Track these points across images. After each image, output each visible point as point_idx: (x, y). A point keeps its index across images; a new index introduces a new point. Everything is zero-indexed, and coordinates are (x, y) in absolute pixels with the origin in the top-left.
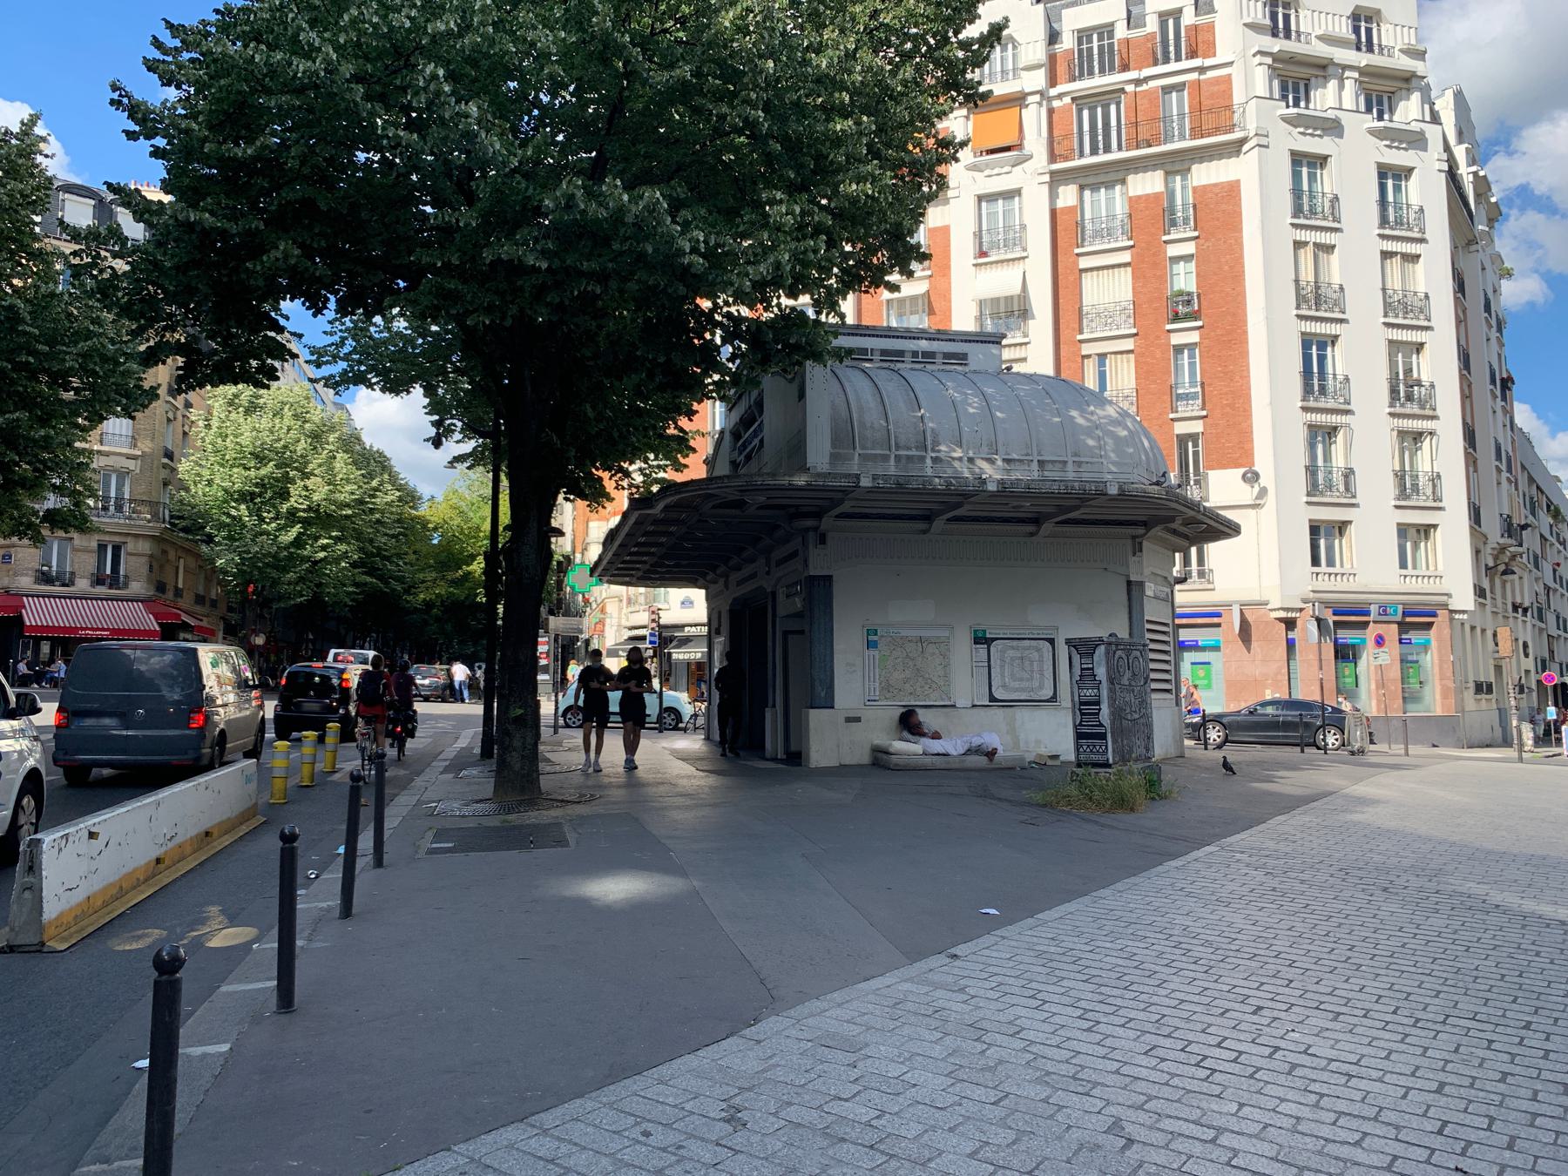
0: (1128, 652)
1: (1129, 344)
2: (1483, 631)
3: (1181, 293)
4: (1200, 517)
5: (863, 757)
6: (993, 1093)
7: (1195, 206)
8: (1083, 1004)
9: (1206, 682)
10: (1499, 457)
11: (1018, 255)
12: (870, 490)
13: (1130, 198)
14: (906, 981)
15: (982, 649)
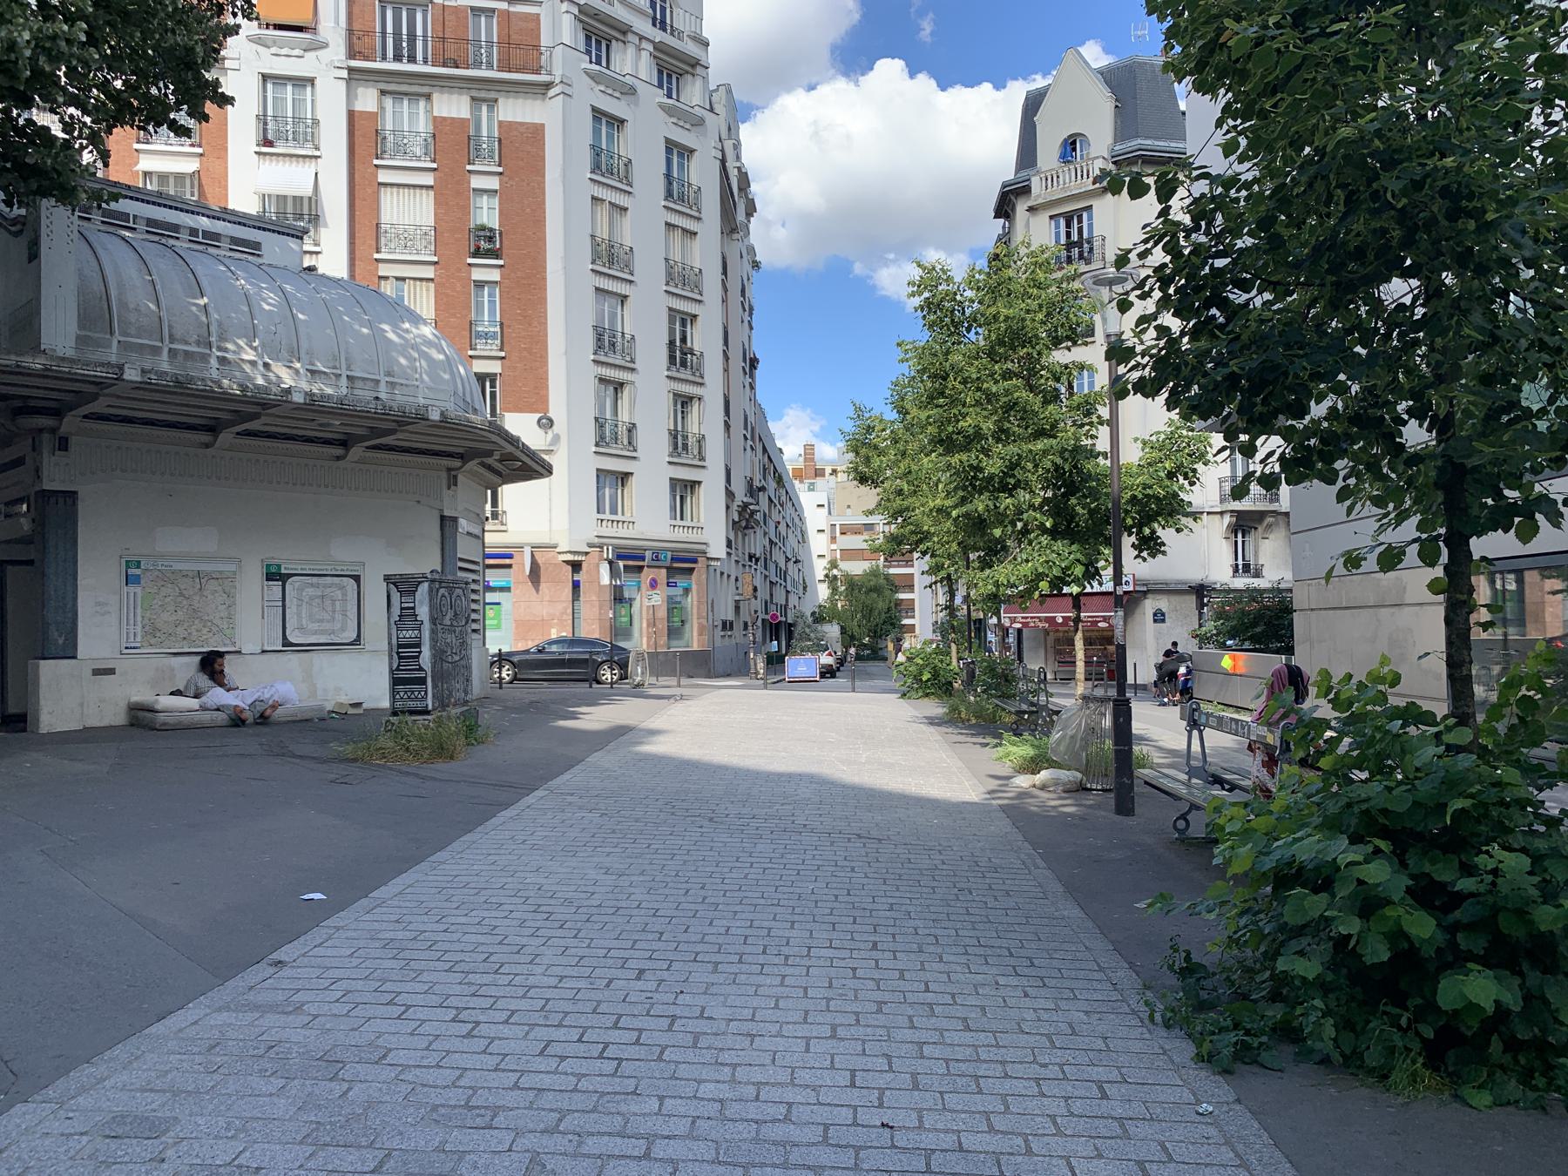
0: (451, 590)
1: (429, 272)
2: (729, 576)
3: (483, 228)
4: (518, 454)
5: (118, 718)
6: (368, 1154)
7: (500, 141)
8: (453, 1001)
9: (495, 622)
10: (746, 428)
11: (310, 153)
12: (138, 386)
13: (435, 118)
14: (219, 1010)
15: (276, 587)
